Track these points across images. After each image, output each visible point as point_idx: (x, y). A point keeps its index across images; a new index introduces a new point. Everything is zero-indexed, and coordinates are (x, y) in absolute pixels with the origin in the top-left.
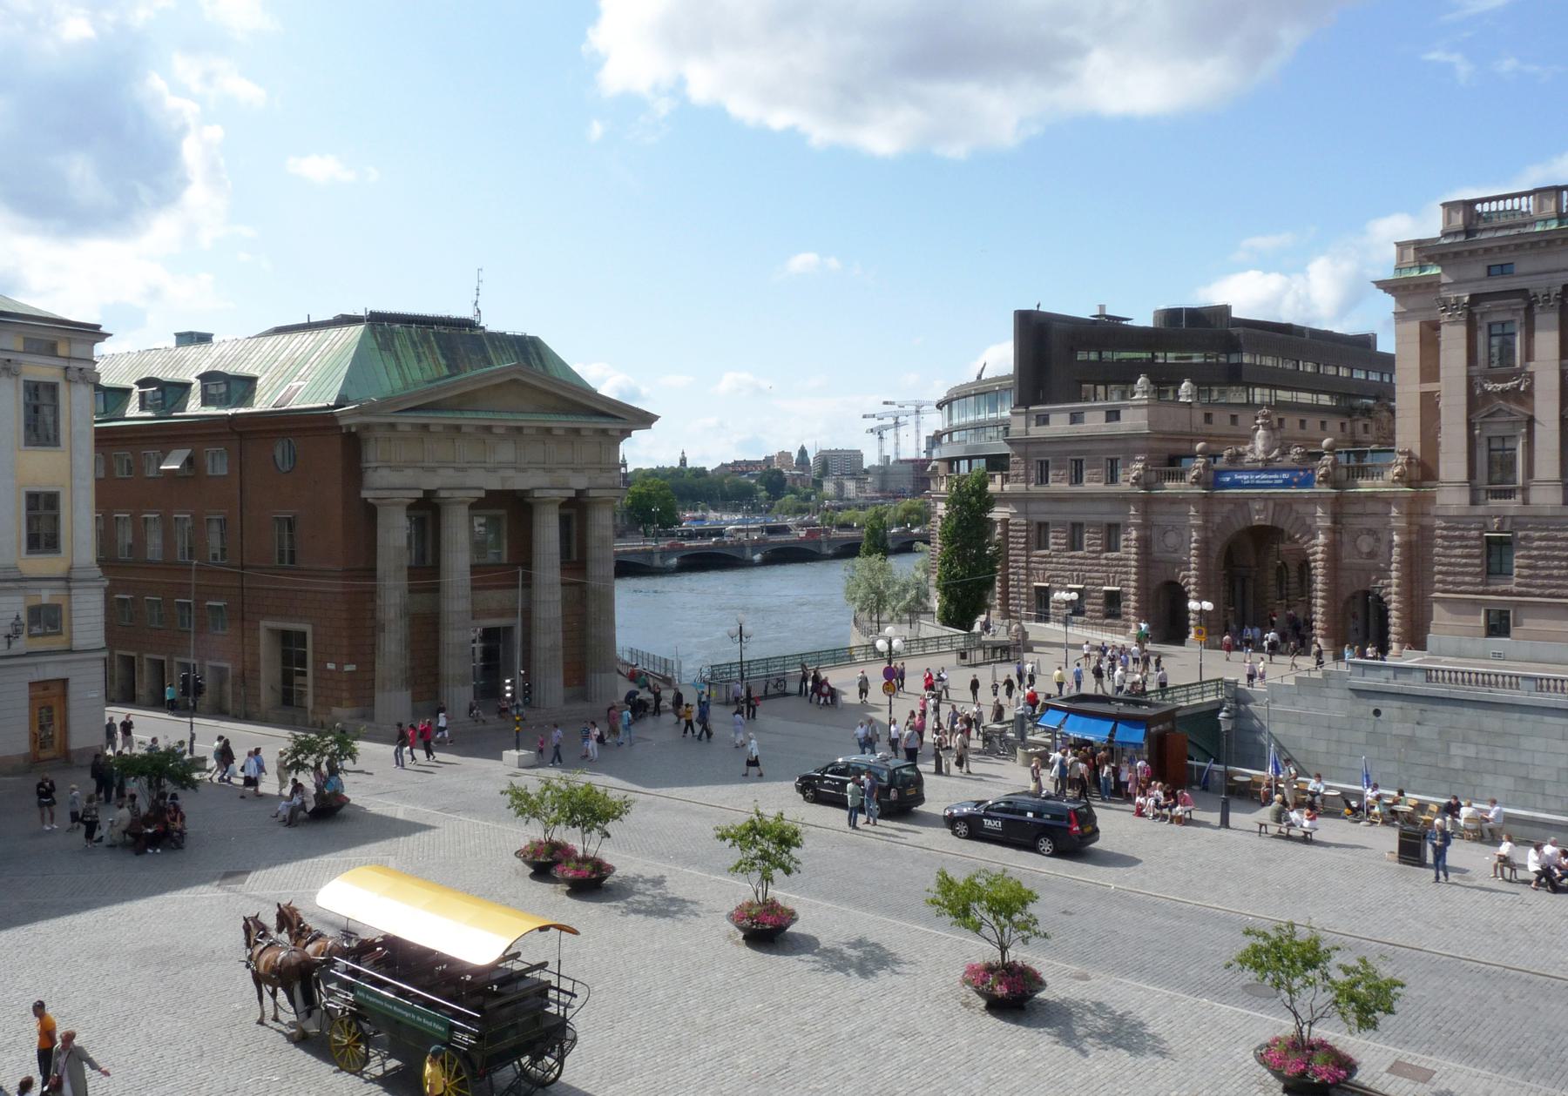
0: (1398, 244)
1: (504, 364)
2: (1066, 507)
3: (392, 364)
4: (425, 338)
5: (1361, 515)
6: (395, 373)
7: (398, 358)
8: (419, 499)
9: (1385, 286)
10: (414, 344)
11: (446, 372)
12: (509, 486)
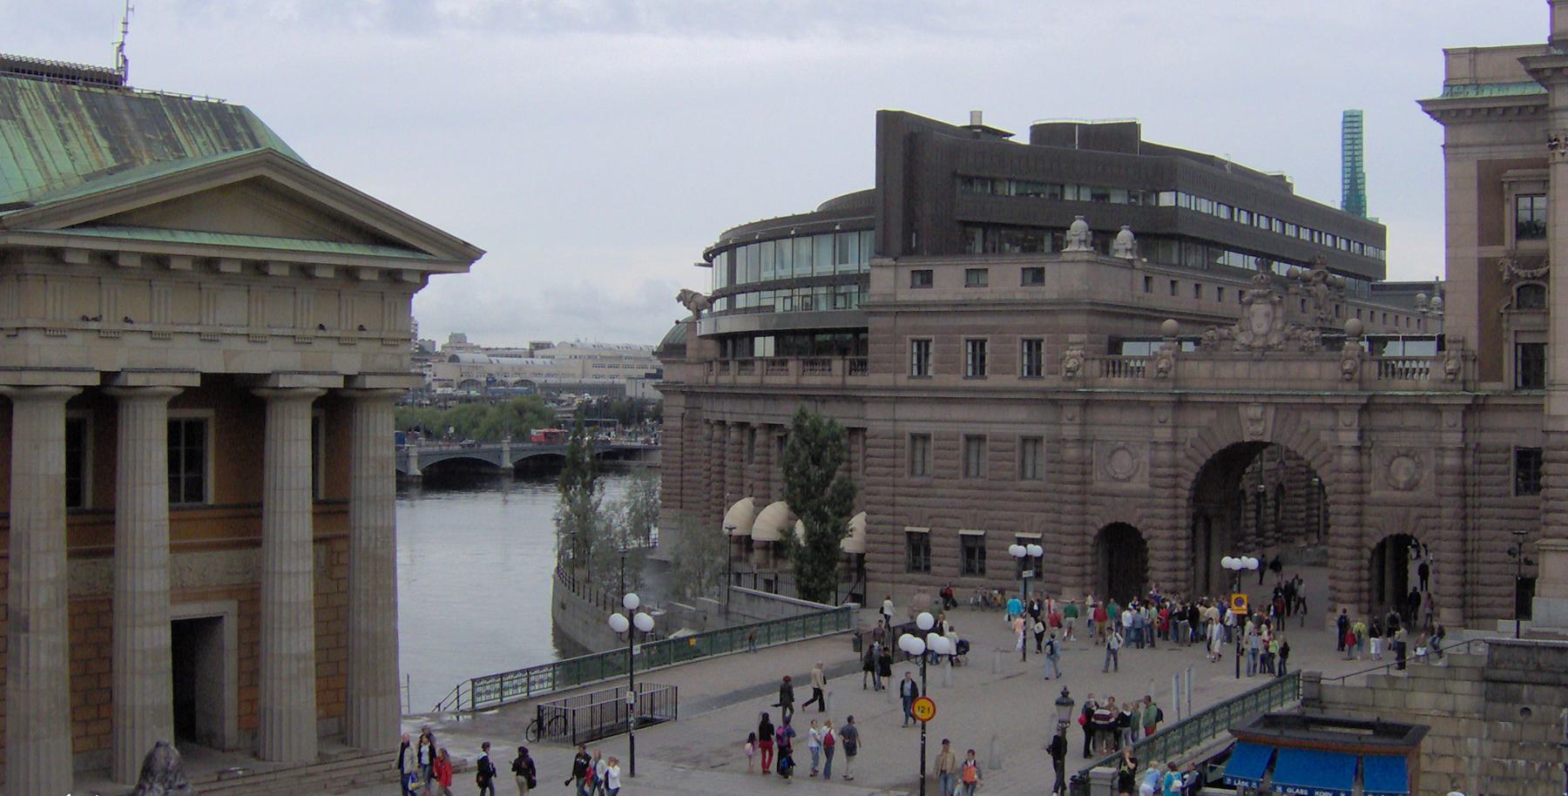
0: (1446, 52)
1: (201, 153)
2: (958, 412)
3: (20, 142)
4: (68, 101)
5: (1399, 429)
6: (28, 160)
7: (28, 133)
8: (332, 391)
9: (1430, 107)
10: (51, 109)
11: (111, 162)
12: (235, 368)
